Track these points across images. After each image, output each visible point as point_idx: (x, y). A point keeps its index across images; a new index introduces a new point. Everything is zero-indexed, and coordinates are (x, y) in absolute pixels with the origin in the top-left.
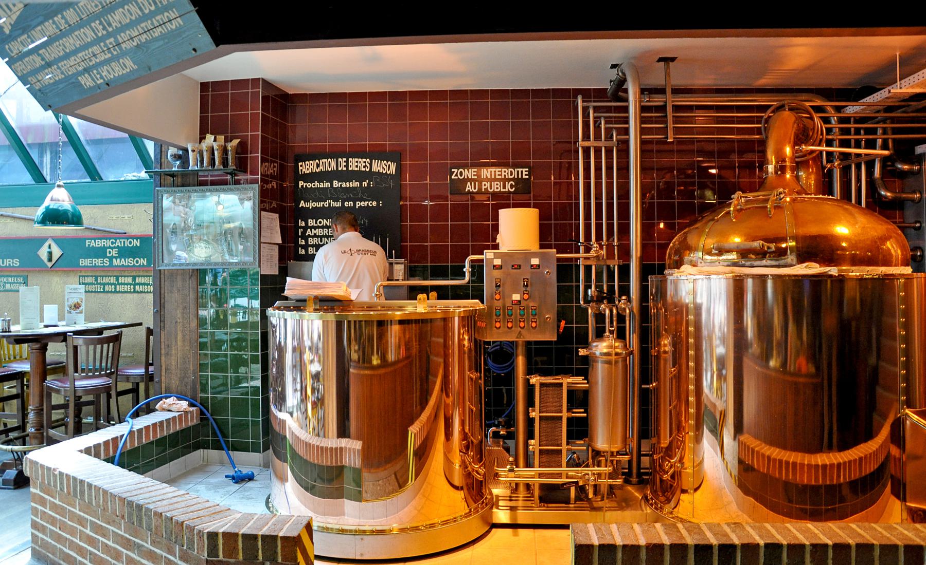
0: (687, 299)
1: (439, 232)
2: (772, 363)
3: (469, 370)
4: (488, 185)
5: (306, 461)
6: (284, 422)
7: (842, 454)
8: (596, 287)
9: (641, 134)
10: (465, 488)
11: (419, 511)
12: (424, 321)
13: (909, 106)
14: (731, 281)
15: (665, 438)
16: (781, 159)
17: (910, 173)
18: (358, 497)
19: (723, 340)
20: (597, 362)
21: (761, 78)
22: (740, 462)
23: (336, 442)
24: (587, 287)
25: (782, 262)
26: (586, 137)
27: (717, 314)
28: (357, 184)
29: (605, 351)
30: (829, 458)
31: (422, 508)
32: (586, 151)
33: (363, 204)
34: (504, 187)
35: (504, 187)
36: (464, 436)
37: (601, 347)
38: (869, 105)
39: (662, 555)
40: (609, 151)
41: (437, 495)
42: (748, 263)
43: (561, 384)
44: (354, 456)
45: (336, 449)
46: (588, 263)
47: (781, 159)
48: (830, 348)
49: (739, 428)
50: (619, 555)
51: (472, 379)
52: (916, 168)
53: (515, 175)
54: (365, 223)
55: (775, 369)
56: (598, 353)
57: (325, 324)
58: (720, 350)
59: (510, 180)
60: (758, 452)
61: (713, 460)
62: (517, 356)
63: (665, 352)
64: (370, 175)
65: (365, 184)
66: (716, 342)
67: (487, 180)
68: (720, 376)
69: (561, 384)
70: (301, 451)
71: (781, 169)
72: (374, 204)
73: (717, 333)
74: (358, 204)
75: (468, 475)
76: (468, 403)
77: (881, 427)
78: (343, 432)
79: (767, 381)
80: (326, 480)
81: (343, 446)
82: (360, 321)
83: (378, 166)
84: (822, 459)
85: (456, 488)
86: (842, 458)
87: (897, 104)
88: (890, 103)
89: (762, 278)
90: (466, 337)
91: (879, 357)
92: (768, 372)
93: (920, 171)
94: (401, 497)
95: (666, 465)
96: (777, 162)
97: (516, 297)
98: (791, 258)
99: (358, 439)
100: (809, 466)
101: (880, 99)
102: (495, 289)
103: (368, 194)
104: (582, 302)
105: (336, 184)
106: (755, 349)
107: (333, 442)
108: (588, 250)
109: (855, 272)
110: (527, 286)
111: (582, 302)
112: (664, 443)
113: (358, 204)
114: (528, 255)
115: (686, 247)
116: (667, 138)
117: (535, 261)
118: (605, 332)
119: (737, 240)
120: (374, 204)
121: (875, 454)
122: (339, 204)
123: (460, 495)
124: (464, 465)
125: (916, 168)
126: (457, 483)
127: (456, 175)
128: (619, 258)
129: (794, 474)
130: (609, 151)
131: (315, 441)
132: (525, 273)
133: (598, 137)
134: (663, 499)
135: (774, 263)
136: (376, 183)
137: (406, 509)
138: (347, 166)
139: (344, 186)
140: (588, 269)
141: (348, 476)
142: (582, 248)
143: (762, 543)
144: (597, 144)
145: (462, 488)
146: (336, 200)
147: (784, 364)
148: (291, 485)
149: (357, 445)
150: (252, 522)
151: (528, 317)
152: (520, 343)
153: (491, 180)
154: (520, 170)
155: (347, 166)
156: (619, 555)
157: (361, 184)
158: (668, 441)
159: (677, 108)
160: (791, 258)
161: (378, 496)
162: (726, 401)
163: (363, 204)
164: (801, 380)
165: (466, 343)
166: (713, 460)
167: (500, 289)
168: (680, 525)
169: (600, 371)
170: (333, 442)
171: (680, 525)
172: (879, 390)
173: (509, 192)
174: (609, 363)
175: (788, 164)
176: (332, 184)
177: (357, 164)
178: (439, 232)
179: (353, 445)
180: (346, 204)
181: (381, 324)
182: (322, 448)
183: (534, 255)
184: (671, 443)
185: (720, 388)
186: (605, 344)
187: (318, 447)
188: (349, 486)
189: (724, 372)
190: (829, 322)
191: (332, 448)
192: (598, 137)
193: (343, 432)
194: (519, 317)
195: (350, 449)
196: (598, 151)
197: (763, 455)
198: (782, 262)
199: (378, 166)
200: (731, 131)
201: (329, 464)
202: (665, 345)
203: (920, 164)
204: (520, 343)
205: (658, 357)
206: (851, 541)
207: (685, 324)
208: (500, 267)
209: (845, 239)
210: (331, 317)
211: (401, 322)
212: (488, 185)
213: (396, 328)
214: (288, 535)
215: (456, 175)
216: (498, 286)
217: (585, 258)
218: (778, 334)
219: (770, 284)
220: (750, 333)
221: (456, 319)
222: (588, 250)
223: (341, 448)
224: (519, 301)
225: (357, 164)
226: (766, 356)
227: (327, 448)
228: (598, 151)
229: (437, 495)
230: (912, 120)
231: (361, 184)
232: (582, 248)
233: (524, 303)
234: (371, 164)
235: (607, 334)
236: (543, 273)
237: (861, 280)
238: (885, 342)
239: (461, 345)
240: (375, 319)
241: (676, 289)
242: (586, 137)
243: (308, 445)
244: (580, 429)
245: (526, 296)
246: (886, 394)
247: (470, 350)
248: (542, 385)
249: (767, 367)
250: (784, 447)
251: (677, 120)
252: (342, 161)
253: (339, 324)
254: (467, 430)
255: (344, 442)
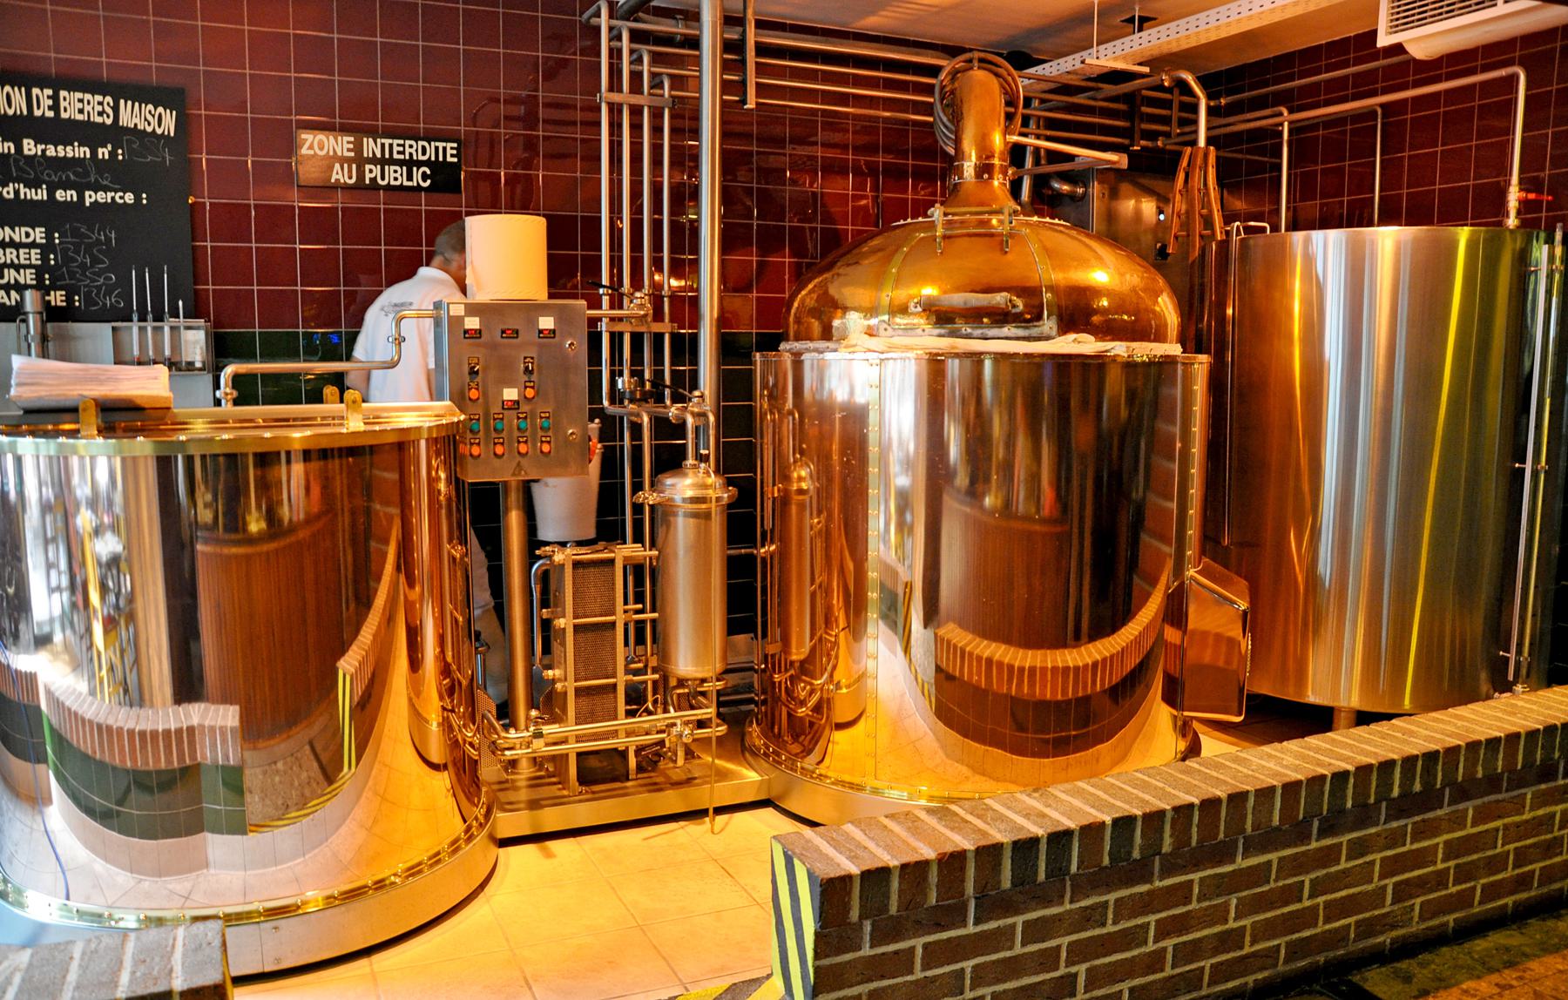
0: (841, 395)
1: (275, 267)
2: (988, 501)
3: (450, 542)
4: (377, 170)
5: (101, 764)
6: (31, 679)
7: (1098, 644)
8: (632, 374)
9: (723, 92)
10: (450, 767)
11: (369, 830)
12: (353, 451)
13: (1098, 89)
14: (924, 363)
15: (800, 644)
16: (985, 153)
17: (1072, 197)
18: (238, 826)
19: (908, 465)
20: (675, 514)
21: (873, 13)
22: (938, 669)
23: (176, 715)
24: (613, 376)
25: (1034, 332)
26: (615, 85)
27: (898, 423)
28: (83, 152)
29: (689, 493)
30: (1081, 655)
31: (375, 821)
32: (615, 109)
33: (101, 197)
34: (410, 178)
35: (410, 178)
36: (445, 671)
37: (683, 487)
38: (1040, 79)
39: (963, 869)
40: (657, 115)
41: (402, 793)
42: (978, 332)
43: (612, 562)
44: (224, 741)
45: (179, 731)
46: (618, 328)
47: (985, 153)
48: (1083, 477)
49: (931, 614)
50: (895, 884)
51: (454, 559)
52: (1080, 191)
53: (431, 154)
54: (108, 239)
55: (992, 512)
56: (678, 498)
57: (130, 464)
58: (902, 481)
59: (420, 164)
60: (971, 654)
61: (888, 670)
62: (507, 510)
63: (801, 492)
64: (115, 133)
65: (103, 153)
66: (895, 468)
67: (374, 160)
68: (901, 525)
69: (612, 562)
70: (86, 743)
71: (984, 170)
72: (129, 198)
73: (895, 456)
74: (90, 197)
75: (455, 744)
76: (449, 606)
77: (1146, 597)
78: (187, 687)
79: (983, 534)
80: (149, 799)
81: (195, 721)
82: (215, 456)
83: (132, 115)
84: (1071, 657)
85: (435, 767)
86: (1100, 653)
87: (1083, 84)
88: (1074, 81)
89: (976, 358)
90: (443, 475)
91: (1147, 486)
92: (985, 518)
93: (1085, 194)
94: (330, 809)
95: (801, 691)
96: (979, 157)
97: (510, 394)
98: (1049, 325)
99: (225, 699)
100: (1055, 669)
101: (1055, 73)
102: (468, 379)
103: (116, 175)
104: (606, 403)
105: (29, 147)
106: (962, 480)
107: (166, 716)
108: (616, 303)
109: (1119, 349)
110: (531, 372)
111: (606, 403)
112: (797, 654)
113: (90, 197)
114: (531, 309)
115: (828, 308)
116: (744, 102)
117: (547, 323)
118: (685, 458)
119: (930, 291)
120: (129, 198)
121: (1138, 640)
122: (41, 195)
123: (443, 781)
124: (447, 726)
125: (1080, 191)
126: (435, 759)
127: (311, 147)
128: (672, 321)
129: (1032, 684)
130: (657, 115)
131: (127, 719)
132: (525, 349)
133: (636, 87)
134: (795, 748)
135: (1021, 332)
136: (130, 152)
137: (343, 830)
138: (55, 107)
139: (51, 152)
140: (616, 339)
141: (212, 785)
142: (605, 300)
143: (1108, 820)
144: (636, 100)
145: (445, 767)
146: (34, 184)
147: (1007, 504)
148: (59, 813)
149: (227, 716)
150: (74, 967)
151: (534, 433)
152: (514, 484)
153: (383, 162)
154: (441, 145)
155: (55, 107)
156: (895, 884)
157: (94, 153)
158: (808, 645)
159: (762, 50)
160: (1049, 325)
161: (281, 813)
162: (911, 567)
163: (101, 197)
164: (1037, 528)
165: (442, 486)
166: (888, 670)
167: (479, 379)
168: (954, 807)
169: (683, 530)
170: (166, 716)
171: (954, 807)
172: (1145, 538)
173: (419, 188)
174: (696, 515)
175: (996, 162)
176: (19, 148)
177: (77, 106)
178: (275, 267)
179: (216, 718)
180: (60, 195)
181: (266, 459)
182: (142, 734)
183: (541, 309)
184: (813, 650)
185: (901, 545)
186: (688, 481)
187: (131, 732)
188: (216, 804)
189: (908, 517)
190: (1082, 434)
191: (167, 733)
192: (636, 87)
193: (187, 687)
194: (516, 433)
195: (212, 729)
196: (636, 111)
197: (979, 658)
198: (1034, 332)
199: (132, 115)
200: (843, 99)
201: (163, 765)
202: (800, 479)
203: (1086, 186)
204: (514, 484)
205: (784, 501)
206: (1219, 793)
207: (845, 444)
208: (477, 334)
209: (1108, 293)
210: (142, 446)
211: (307, 455)
212: (377, 170)
213: (298, 468)
214: (194, 985)
215: (311, 147)
216: (473, 373)
217: (612, 319)
218: (999, 453)
219: (988, 365)
220: (954, 451)
221: (423, 443)
222: (616, 303)
223: (191, 730)
224: (517, 402)
225: (77, 106)
226: (974, 492)
227: (154, 734)
228: (636, 111)
229: (402, 793)
230: (1104, 113)
231: (94, 153)
232: (605, 300)
233: (525, 408)
234: (116, 109)
235: (690, 461)
236: (561, 346)
237: (1130, 366)
238: (1159, 462)
239: (434, 493)
240: (251, 450)
241: (821, 381)
242: (615, 85)
243: (106, 732)
244: (650, 636)
245: (530, 393)
246: (1156, 543)
247: (449, 500)
248: (577, 565)
249: (982, 507)
250: (1007, 640)
251: (761, 70)
252: (43, 95)
253: (164, 465)
254: (449, 659)
255: (195, 714)
